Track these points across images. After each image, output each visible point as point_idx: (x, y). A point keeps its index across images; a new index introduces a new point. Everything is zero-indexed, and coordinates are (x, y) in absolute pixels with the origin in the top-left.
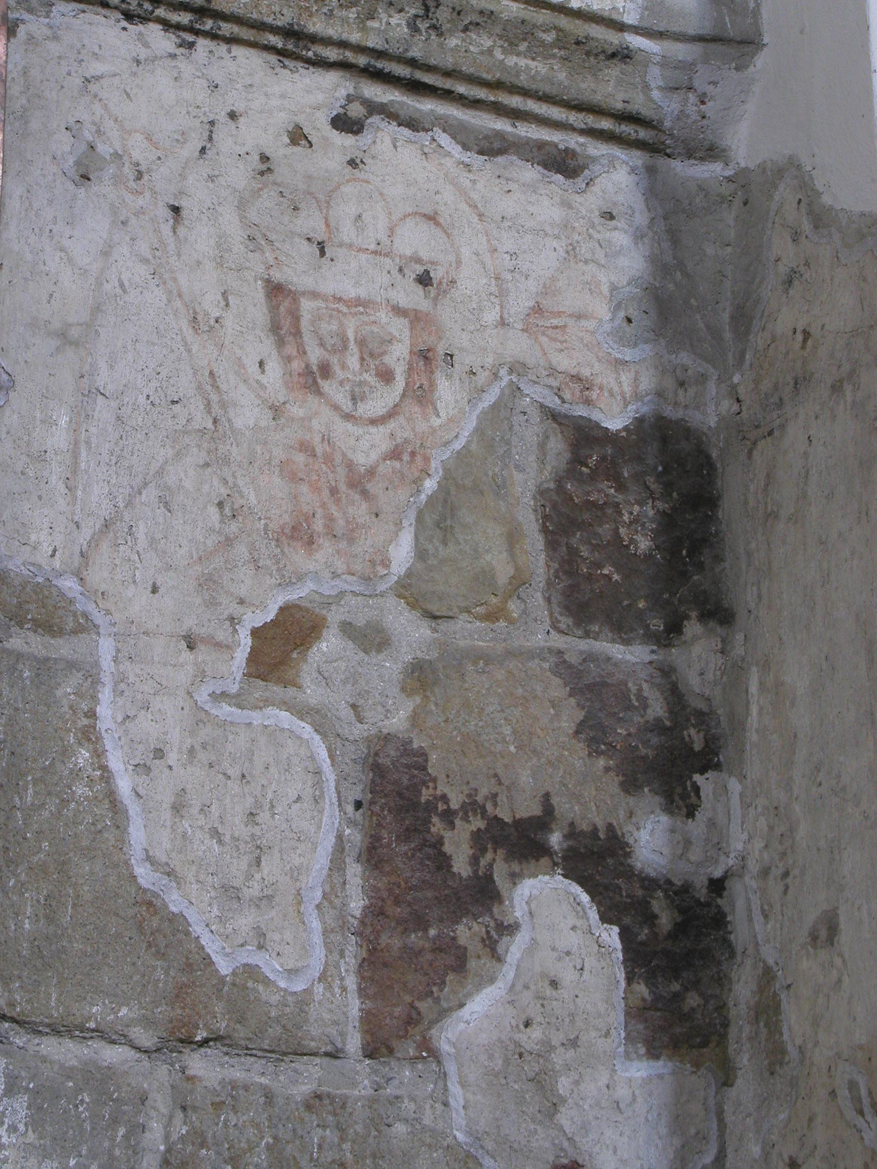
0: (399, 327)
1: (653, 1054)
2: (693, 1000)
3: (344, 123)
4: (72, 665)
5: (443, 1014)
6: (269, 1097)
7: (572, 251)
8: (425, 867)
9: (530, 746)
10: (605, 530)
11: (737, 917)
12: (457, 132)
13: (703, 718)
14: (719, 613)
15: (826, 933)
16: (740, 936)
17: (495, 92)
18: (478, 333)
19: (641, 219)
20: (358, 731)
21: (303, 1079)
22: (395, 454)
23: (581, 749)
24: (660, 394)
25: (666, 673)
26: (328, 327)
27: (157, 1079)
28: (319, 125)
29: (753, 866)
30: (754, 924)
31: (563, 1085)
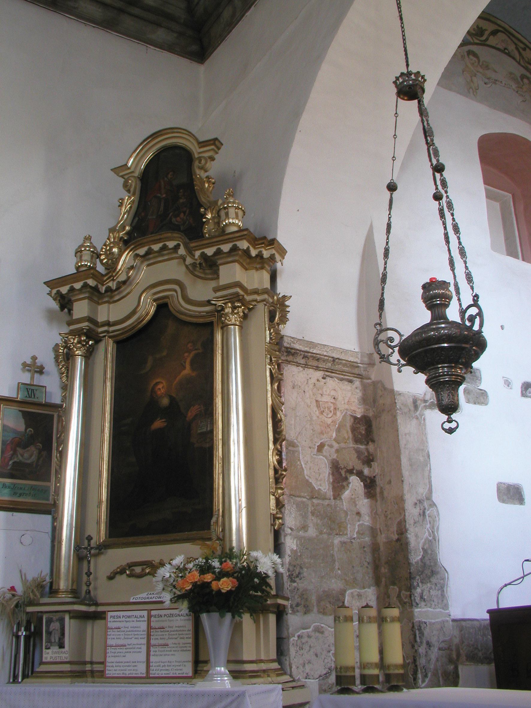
0: (332, 405)
1: (368, 498)
2: (372, 491)
3: (324, 378)
4: (297, 451)
5: (342, 494)
6: (323, 504)
7: (352, 393)
8: (339, 475)
9: (351, 460)
10: (358, 431)
11: (377, 481)
12: (337, 378)
13: (372, 455)
14: (373, 441)
15: (390, 482)
16: (377, 483)
17: (342, 372)
18: (342, 406)
19: (361, 388)
20: (330, 458)
21: (326, 502)
22: (332, 422)
23: (357, 459)
24: (364, 412)
25: (367, 450)
26: (323, 406)
27: (309, 503)
28: (321, 379)
29: (379, 474)
30: (379, 482)
31: (357, 503)
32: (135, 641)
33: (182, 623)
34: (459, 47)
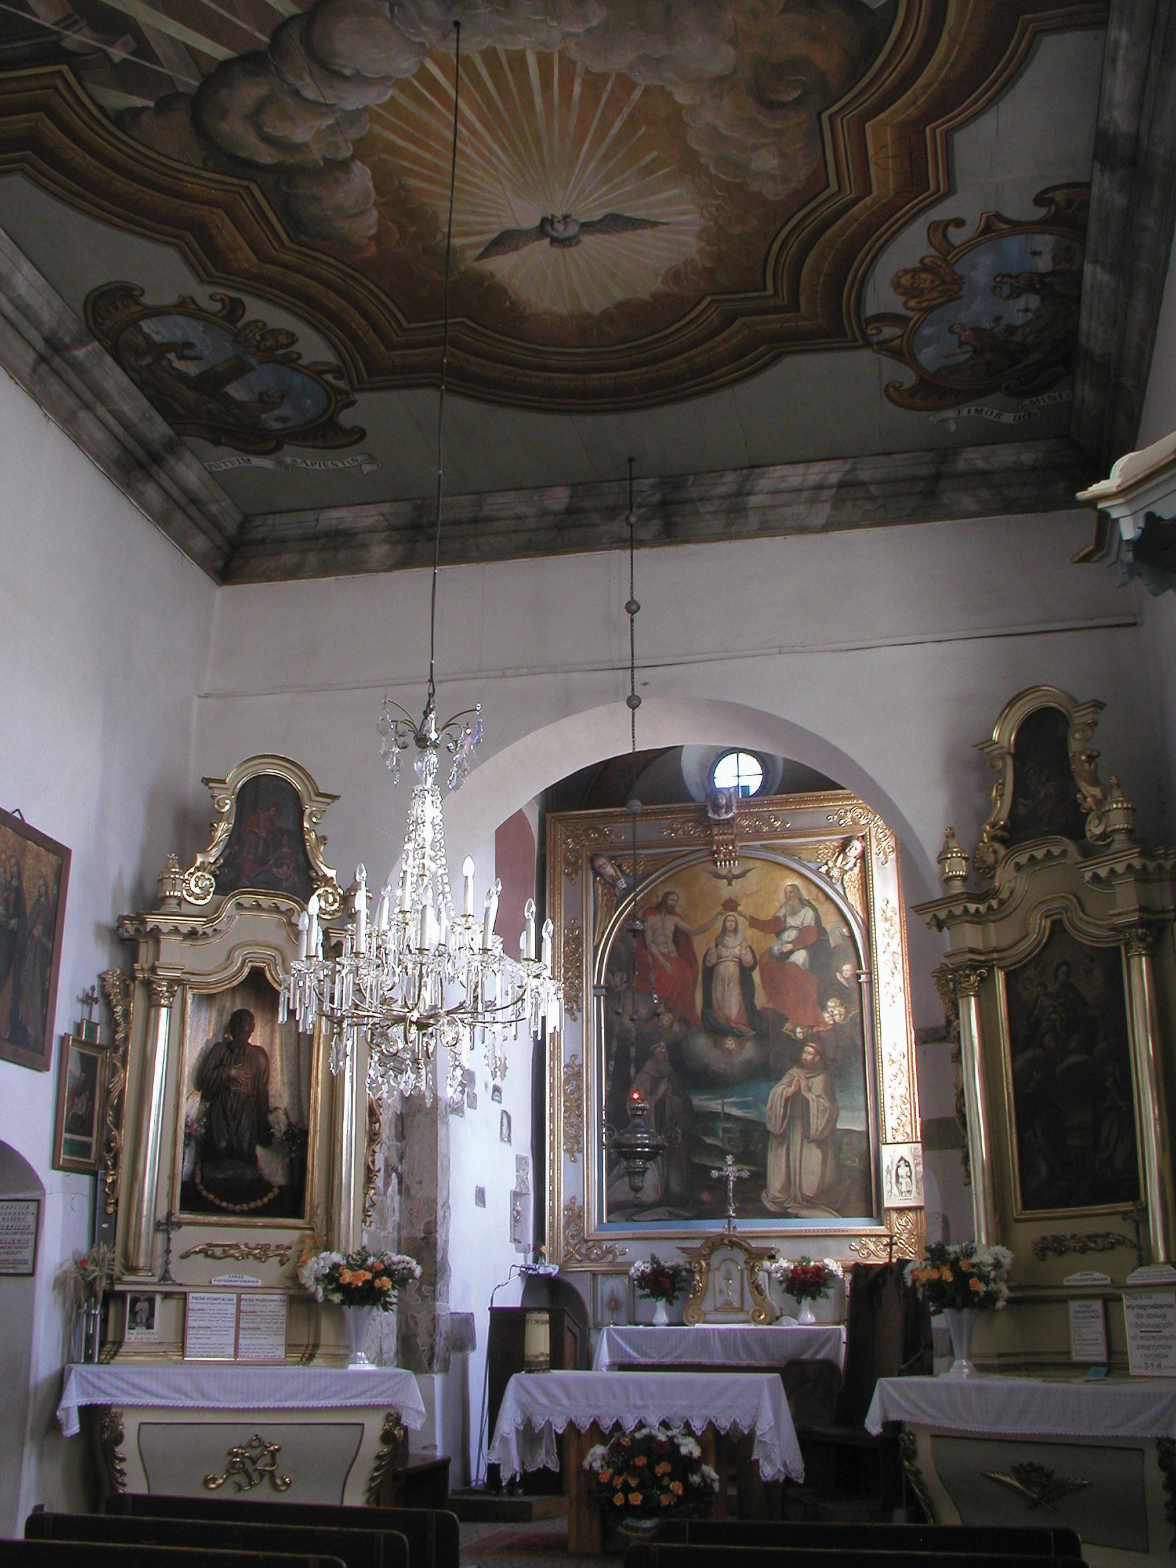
15: (420, 1182)
32: (221, 1324)
33: (273, 1308)
34: (184, 44)
